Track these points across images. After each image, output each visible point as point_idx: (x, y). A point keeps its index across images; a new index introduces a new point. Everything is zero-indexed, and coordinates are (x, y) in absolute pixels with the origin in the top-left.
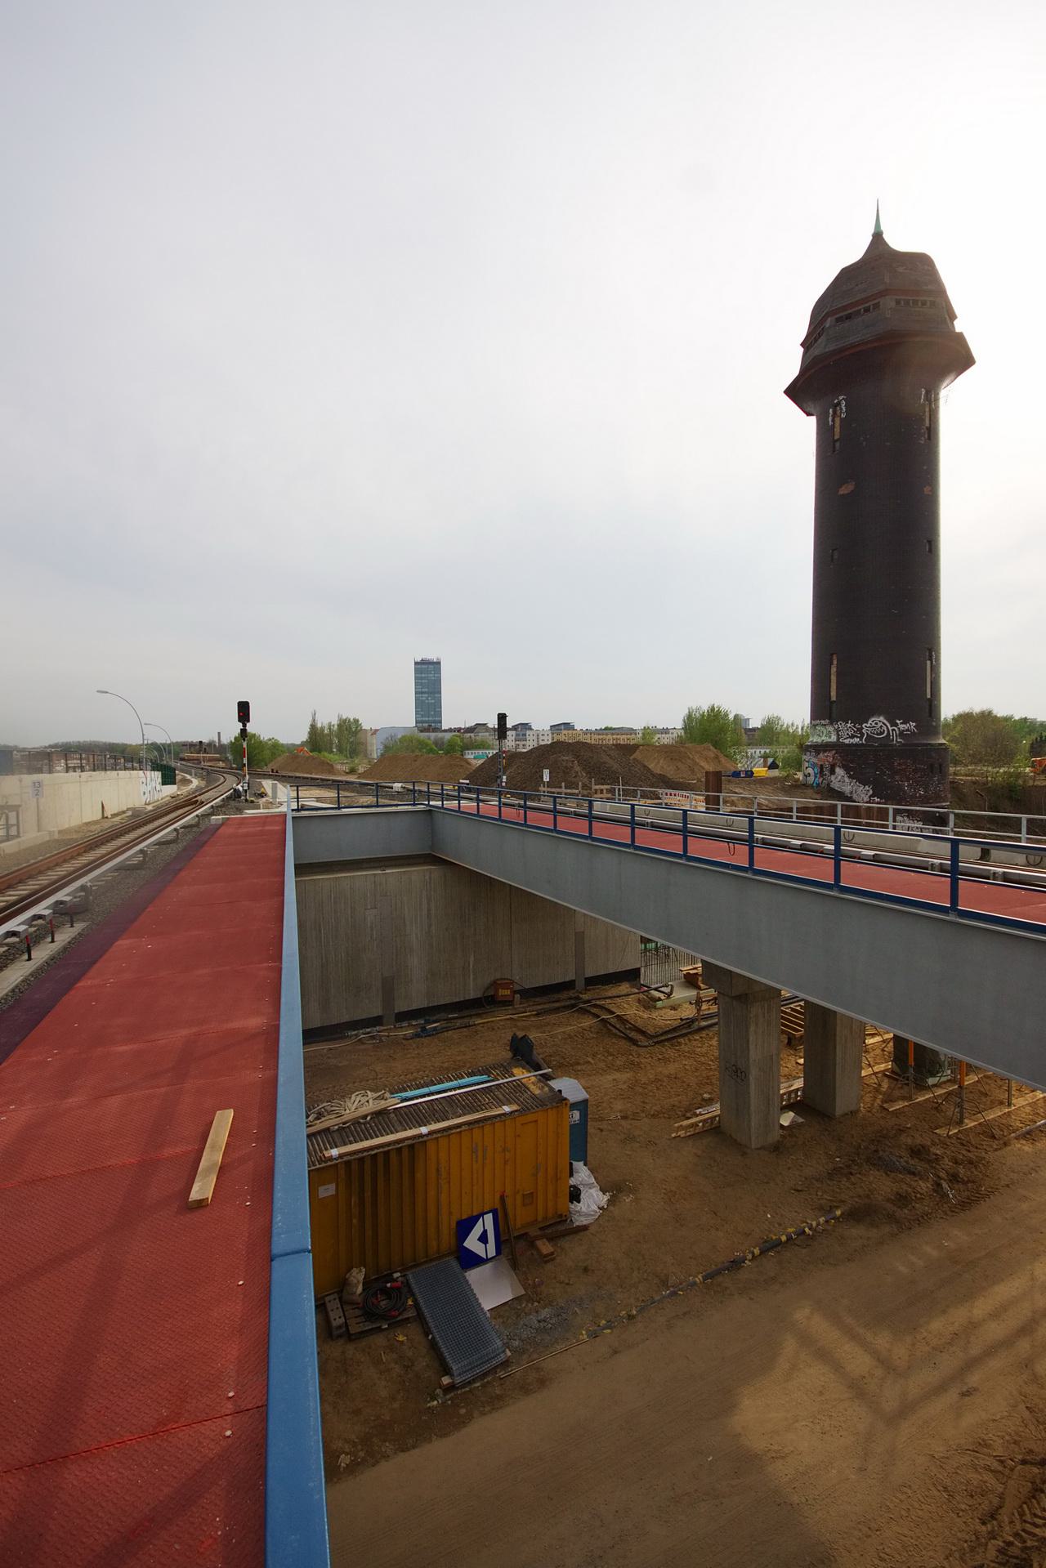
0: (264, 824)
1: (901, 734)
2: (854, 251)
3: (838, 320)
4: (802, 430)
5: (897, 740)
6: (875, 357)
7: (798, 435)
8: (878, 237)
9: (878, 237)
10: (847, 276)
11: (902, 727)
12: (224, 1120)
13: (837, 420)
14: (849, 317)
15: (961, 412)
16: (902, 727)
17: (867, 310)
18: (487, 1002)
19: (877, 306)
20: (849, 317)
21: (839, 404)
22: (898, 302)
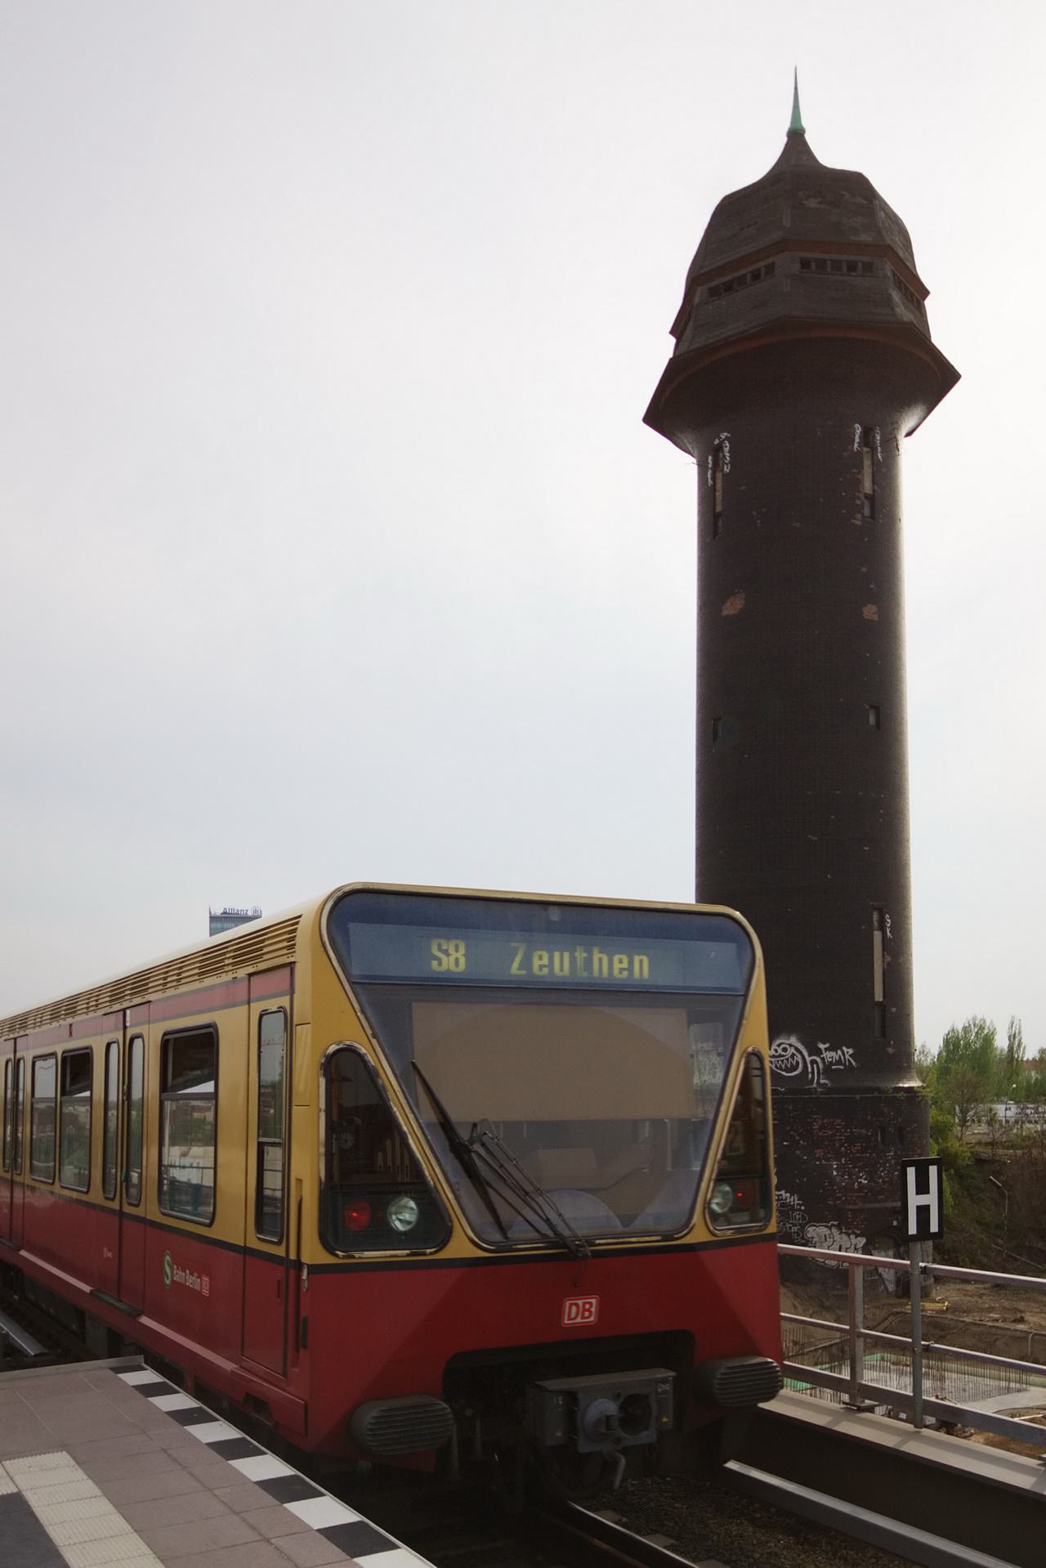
0: (899, 285)
1: (828, 1070)
2: (754, 161)
3: (714, 292)
4: (672, 478)
5: (819, 1081)
6: (796, 346)
7: (668, 486)
8: (796, 136)
9: (796, 136)
10: (734, 212)
11: (830, 1056)
12: (87, 1288)
13: (719, 476)
14: (729, 287)
15: (932, 462)
16: (830, 1056)
17: (756, 276)
18: (175, 1460)
19: (770, 268)
20: (729, 287)
21: (720, 448)
22: (805, 264)
